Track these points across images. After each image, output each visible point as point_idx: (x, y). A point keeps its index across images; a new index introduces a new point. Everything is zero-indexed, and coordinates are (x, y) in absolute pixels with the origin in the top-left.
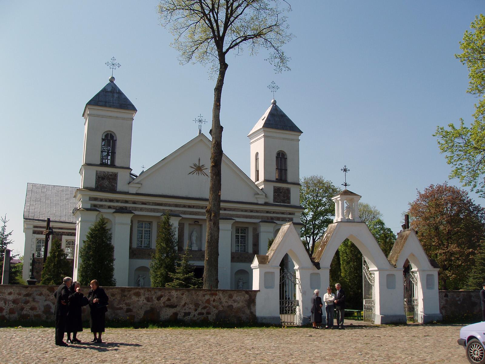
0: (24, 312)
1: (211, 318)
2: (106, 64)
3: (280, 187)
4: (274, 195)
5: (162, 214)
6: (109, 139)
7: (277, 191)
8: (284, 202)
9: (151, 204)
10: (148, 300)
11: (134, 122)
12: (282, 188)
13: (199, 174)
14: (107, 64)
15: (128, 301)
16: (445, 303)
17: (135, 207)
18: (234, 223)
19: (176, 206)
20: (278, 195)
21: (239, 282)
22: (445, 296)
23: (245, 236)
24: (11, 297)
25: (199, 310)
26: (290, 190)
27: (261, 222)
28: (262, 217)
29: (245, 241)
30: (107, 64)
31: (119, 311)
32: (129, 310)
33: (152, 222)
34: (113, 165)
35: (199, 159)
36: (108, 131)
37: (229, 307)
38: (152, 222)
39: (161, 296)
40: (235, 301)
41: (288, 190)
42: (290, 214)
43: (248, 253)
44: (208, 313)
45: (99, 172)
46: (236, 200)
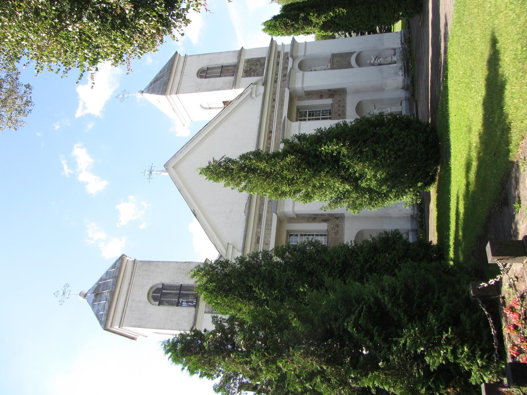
2: (61, 304)
3: (243, 70)
4: (254, 76)
5: (274, 214)
6: (159, 295)
7: (248, 73)
9: (259, 230)
11: (139, 259)
12: (245, 68)
14: (61, 302)
18: (289, 119)
20: (254, 71)
21: (374, 113)
23: (309, 112)
27: (289, 88)
28: (283, 87)
29: (317, 111)
30: (61, 302)
33: (288, 232)
38: (288, 232)
42: (279, 56)
43: (332, 104)
45: (207, 309)
46: (258, 120)
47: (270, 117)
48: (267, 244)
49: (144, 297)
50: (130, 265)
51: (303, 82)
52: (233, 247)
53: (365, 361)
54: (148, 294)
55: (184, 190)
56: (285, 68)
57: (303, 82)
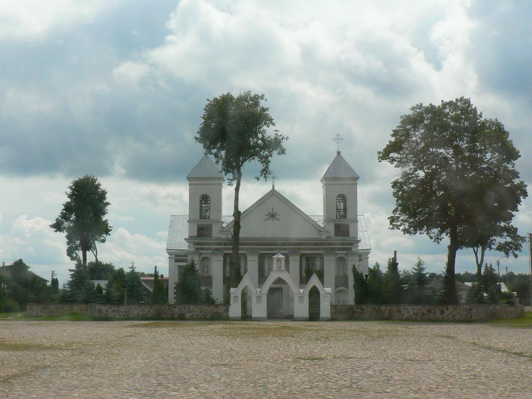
0: (129, 316)
1: (208, 317)
10: (180, 309)
13: (273, 219)
15: (171, 310)
24: (124, 310)
25: (203, 314)
28: (325, 249)
31: (168, 315)
32: (172, 314)
35: (273, 209)
36: (204, 194)
37: (216, 312)
39: (186, 308)
40: (219, 310)
44: (207, 315)
47: (305, 244)
51: (292, 260)
56: (339, 249)
57: (292, 260)
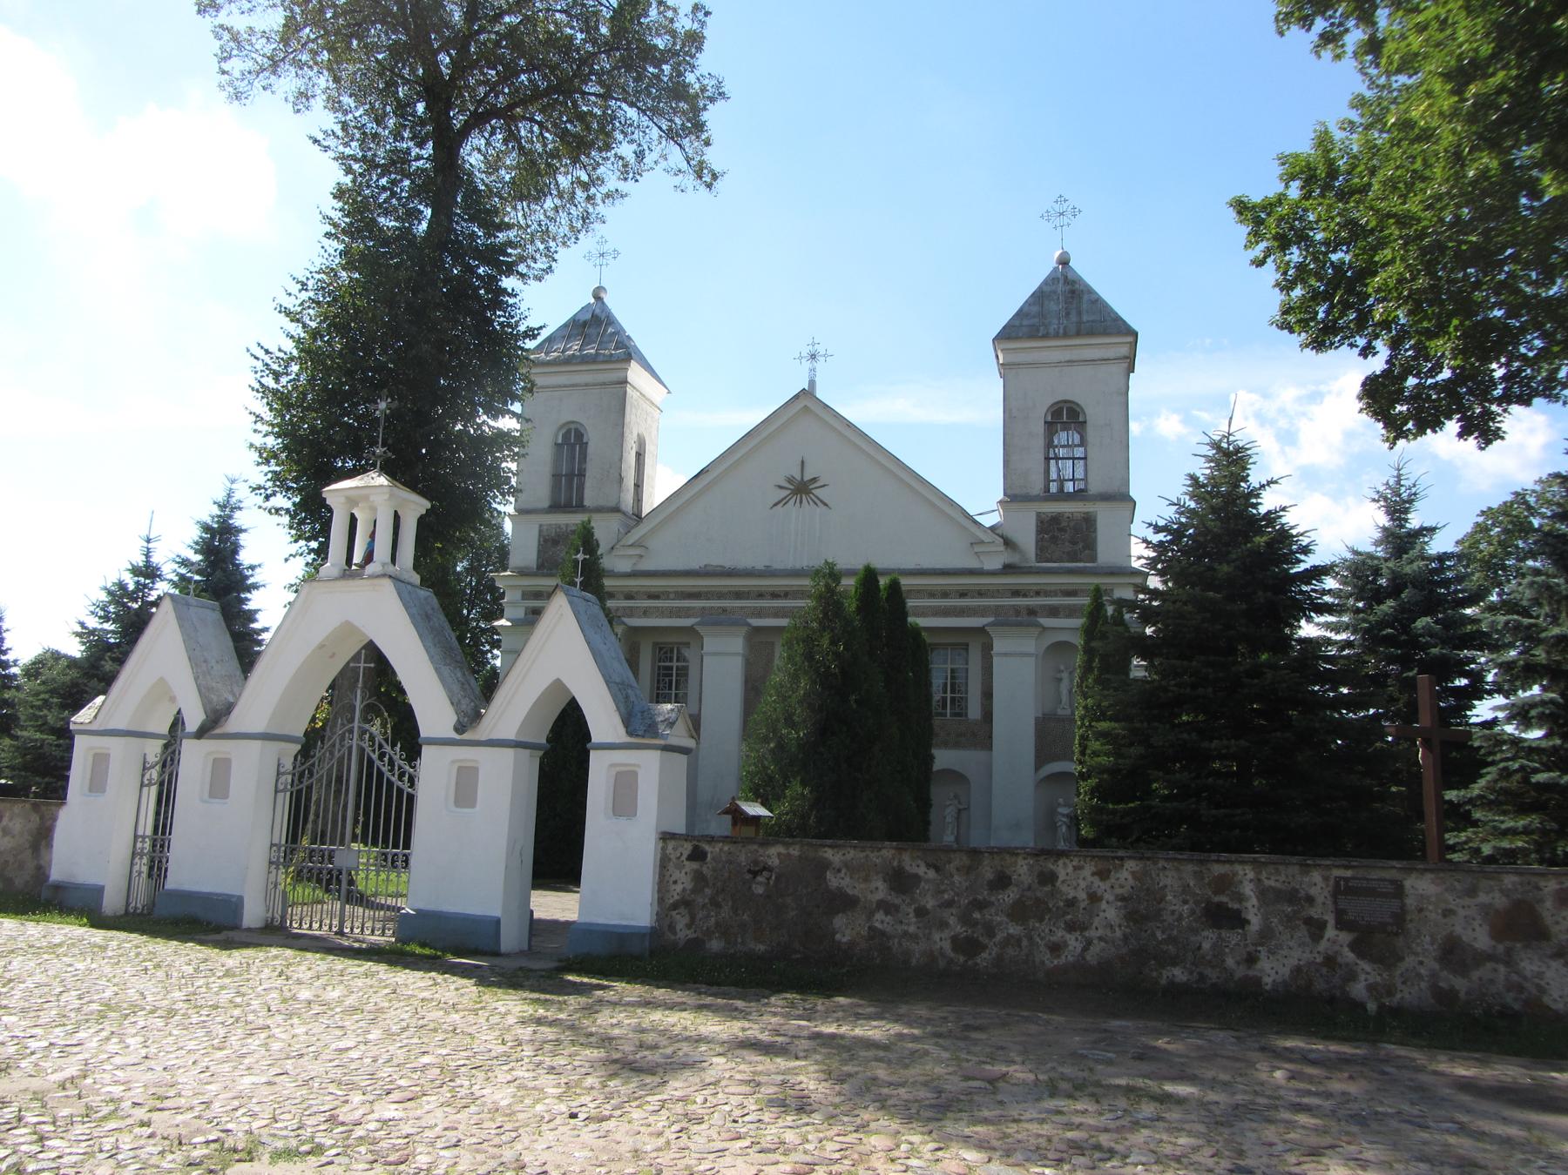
8: (1073, 557)
9: (672, 596)
13: (801, 502)
16: (689, 886)
17: (631, 608)
19: (738, 595)
22: (691, 858)
26: (1095, 521)
28: (997, 611)
34: (580, 507)
35: (803, 462)
41: (1089, 521)
47: (919, 591)
48: (923, 612)
49: (567, 417)
50: (613, 376)
51: (1006, 654)
52: (641, 556)
53: (1170, 919)
54: (573, 422)
55: (751, 444)
56: (1054, 612)
57: (1006, 654)
